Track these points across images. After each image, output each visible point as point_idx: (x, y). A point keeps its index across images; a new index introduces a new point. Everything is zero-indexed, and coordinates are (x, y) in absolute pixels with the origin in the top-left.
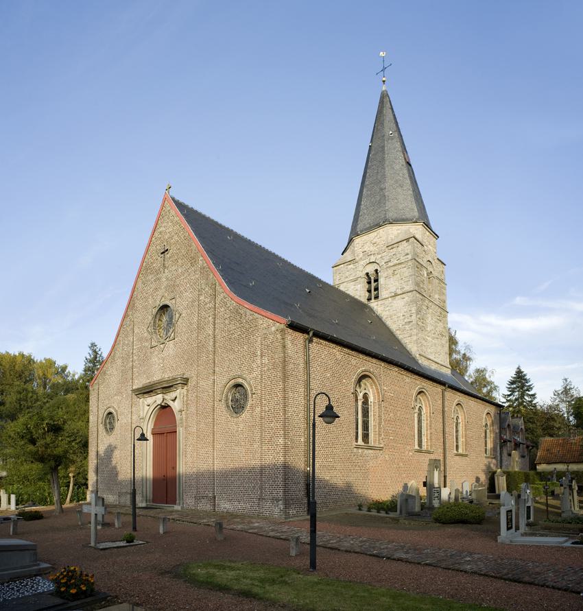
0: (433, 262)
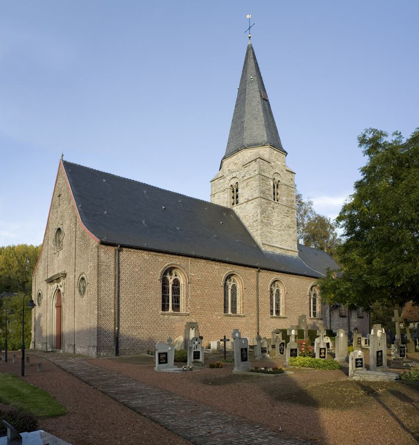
0: (281, 174)
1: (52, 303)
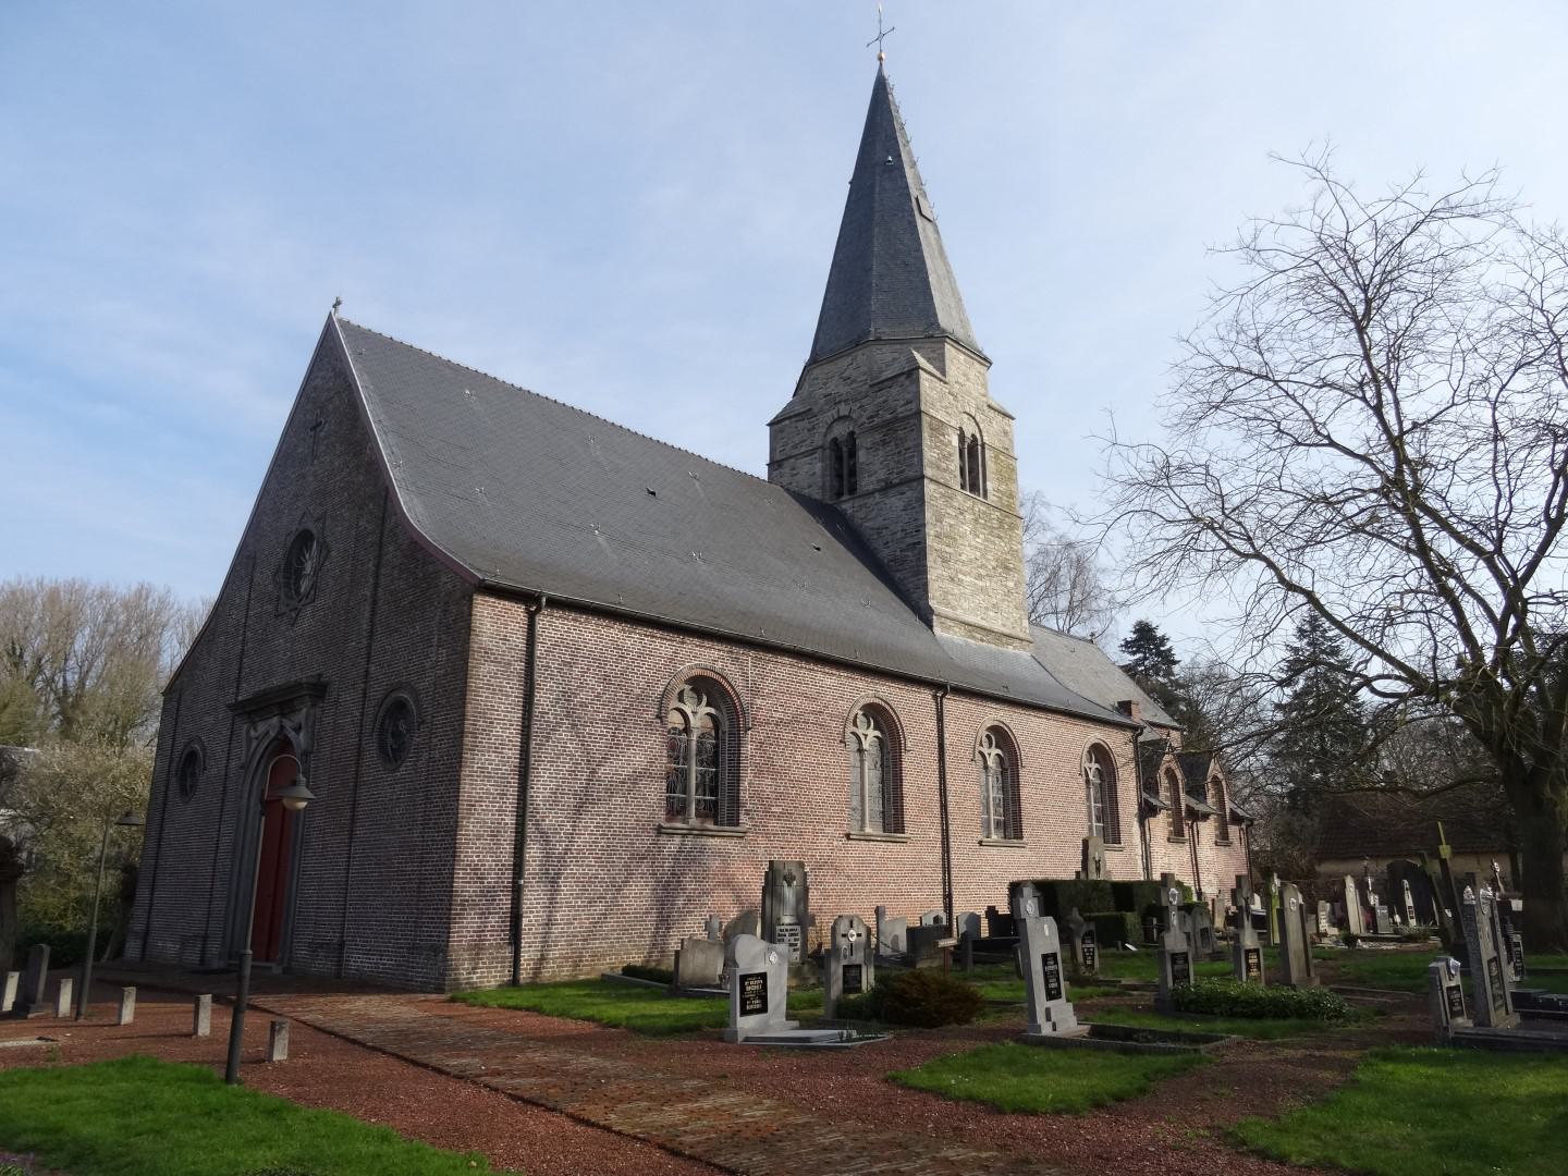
1: (247, 788)
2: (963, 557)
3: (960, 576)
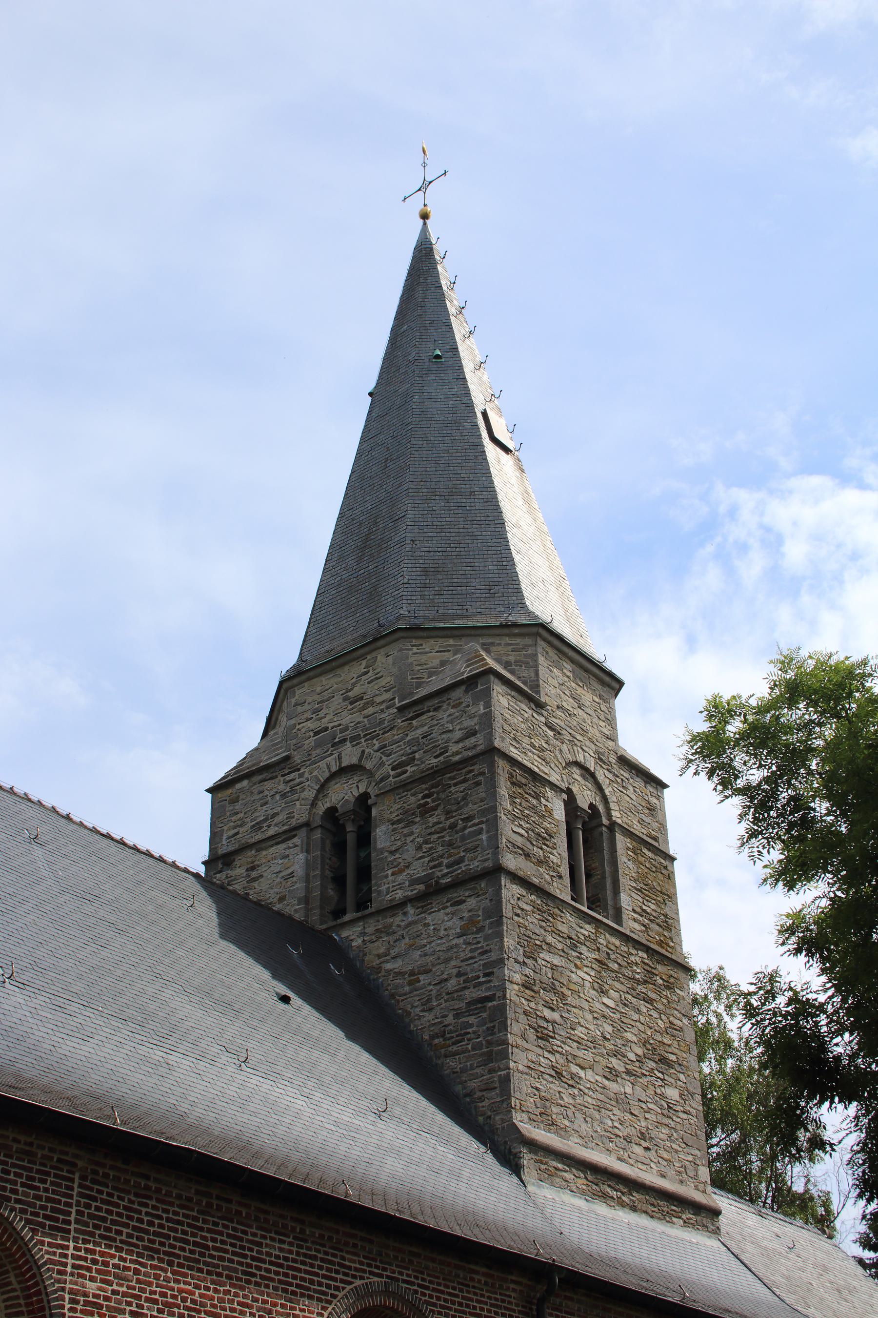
2: (579, 1032)
3: (575, 1069)
